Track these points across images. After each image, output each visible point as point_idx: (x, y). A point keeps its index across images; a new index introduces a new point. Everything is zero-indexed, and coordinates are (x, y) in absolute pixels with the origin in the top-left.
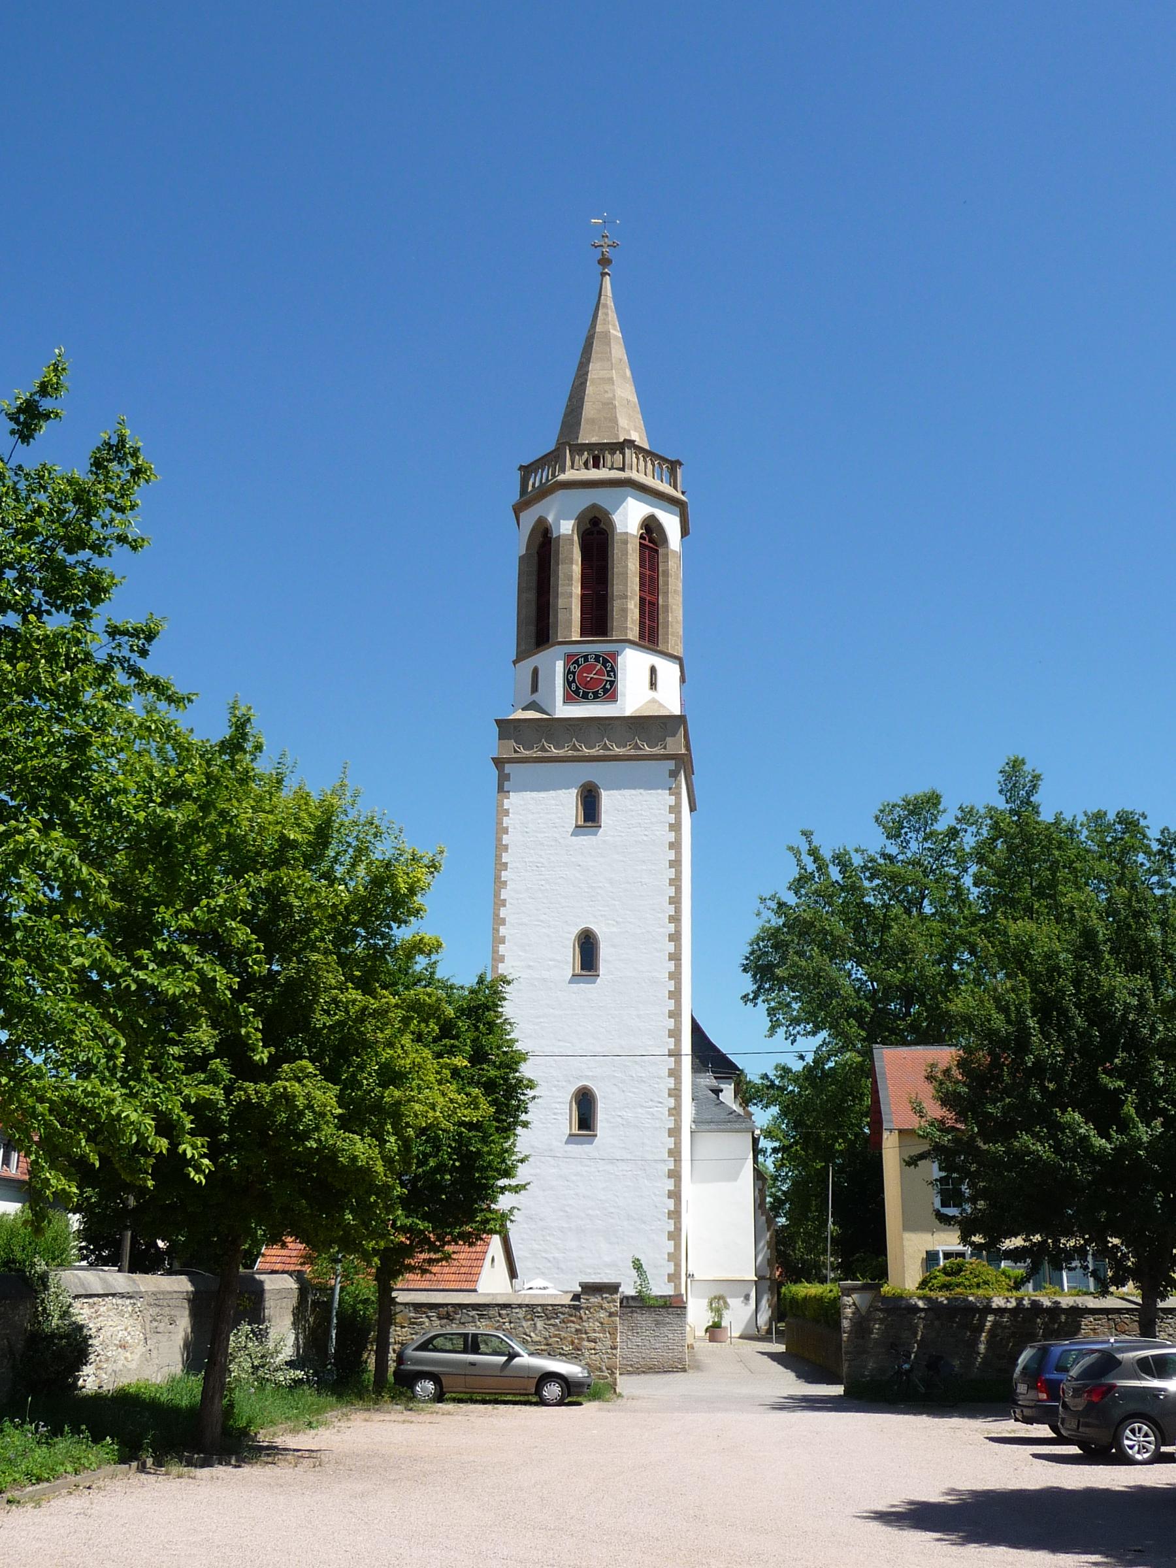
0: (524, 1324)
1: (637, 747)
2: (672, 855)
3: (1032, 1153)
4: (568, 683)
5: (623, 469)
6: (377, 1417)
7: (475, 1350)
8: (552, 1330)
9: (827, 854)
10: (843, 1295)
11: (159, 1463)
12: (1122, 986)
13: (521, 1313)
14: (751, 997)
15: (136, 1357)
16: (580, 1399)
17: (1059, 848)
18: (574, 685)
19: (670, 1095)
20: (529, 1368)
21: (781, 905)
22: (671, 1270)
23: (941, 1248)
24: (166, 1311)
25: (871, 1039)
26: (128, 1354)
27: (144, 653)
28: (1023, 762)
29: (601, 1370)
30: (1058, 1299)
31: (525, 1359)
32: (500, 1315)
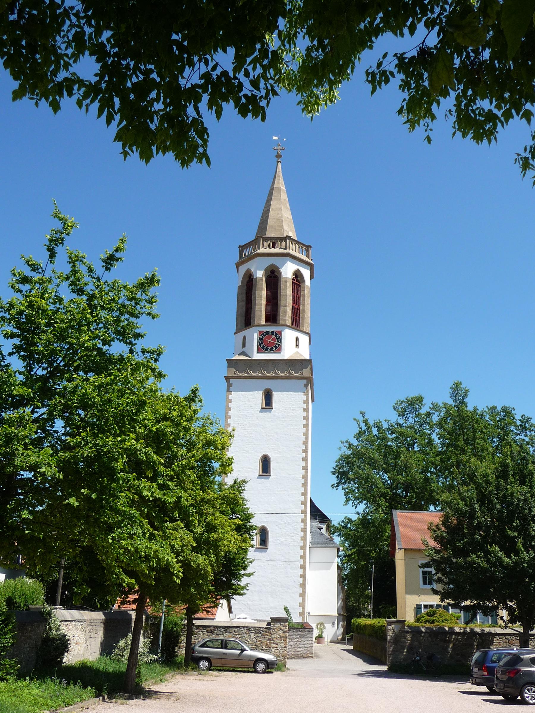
0: (246, 636)
1: (290, 373)
2: (304, 422)
3: (477, 563)
4: (259, 343)
5: (285, 249)
6: (188, 677)
7: (226, 648)
8: (258, 638)
9: (371, 422)
10: (388, 625)
11: (111, 697)
12: (517, 491)
13: (244, 630)
14: (335, 485)
15: (82, 649)
16: (272, 670)
17: (477, 423)
18: (262, 345)
19: (302, 531)
20: (250, 656)
21: (350, 445)
22: (301, 610)
23: (423, 603)
24: (94, 628)
25: (391, 508)
26: (79, 647)
27: (156, 361)
28: (461, 384)
29: (279, 657)
30: (484, 629)
31: (248, 652)
32: (235, 631)
